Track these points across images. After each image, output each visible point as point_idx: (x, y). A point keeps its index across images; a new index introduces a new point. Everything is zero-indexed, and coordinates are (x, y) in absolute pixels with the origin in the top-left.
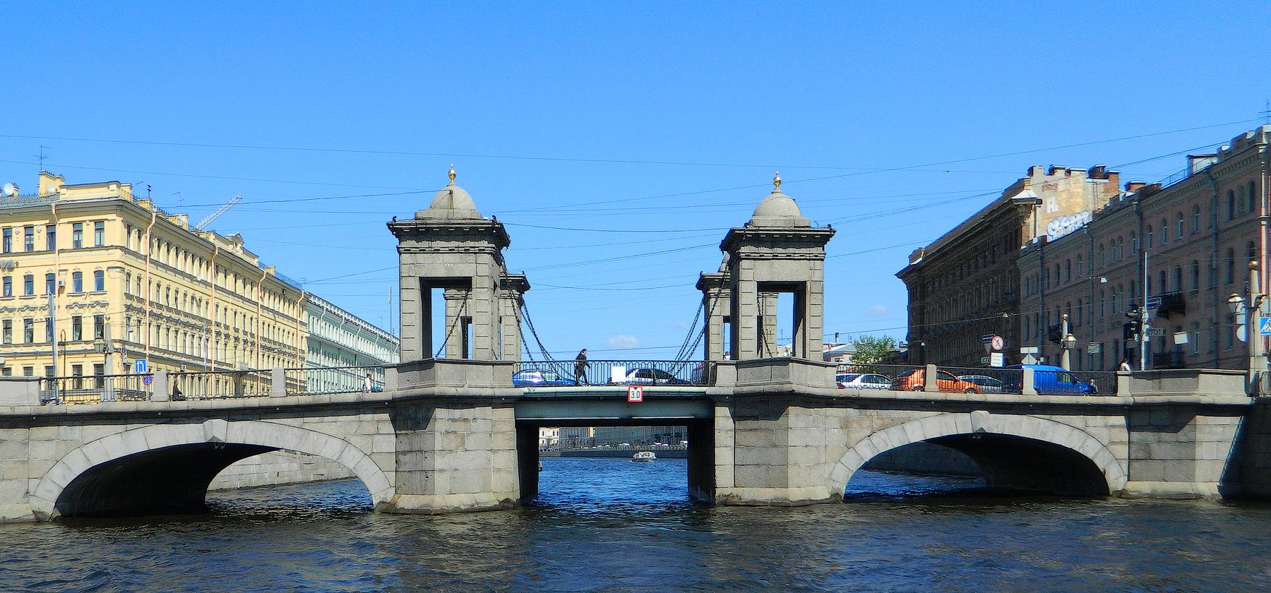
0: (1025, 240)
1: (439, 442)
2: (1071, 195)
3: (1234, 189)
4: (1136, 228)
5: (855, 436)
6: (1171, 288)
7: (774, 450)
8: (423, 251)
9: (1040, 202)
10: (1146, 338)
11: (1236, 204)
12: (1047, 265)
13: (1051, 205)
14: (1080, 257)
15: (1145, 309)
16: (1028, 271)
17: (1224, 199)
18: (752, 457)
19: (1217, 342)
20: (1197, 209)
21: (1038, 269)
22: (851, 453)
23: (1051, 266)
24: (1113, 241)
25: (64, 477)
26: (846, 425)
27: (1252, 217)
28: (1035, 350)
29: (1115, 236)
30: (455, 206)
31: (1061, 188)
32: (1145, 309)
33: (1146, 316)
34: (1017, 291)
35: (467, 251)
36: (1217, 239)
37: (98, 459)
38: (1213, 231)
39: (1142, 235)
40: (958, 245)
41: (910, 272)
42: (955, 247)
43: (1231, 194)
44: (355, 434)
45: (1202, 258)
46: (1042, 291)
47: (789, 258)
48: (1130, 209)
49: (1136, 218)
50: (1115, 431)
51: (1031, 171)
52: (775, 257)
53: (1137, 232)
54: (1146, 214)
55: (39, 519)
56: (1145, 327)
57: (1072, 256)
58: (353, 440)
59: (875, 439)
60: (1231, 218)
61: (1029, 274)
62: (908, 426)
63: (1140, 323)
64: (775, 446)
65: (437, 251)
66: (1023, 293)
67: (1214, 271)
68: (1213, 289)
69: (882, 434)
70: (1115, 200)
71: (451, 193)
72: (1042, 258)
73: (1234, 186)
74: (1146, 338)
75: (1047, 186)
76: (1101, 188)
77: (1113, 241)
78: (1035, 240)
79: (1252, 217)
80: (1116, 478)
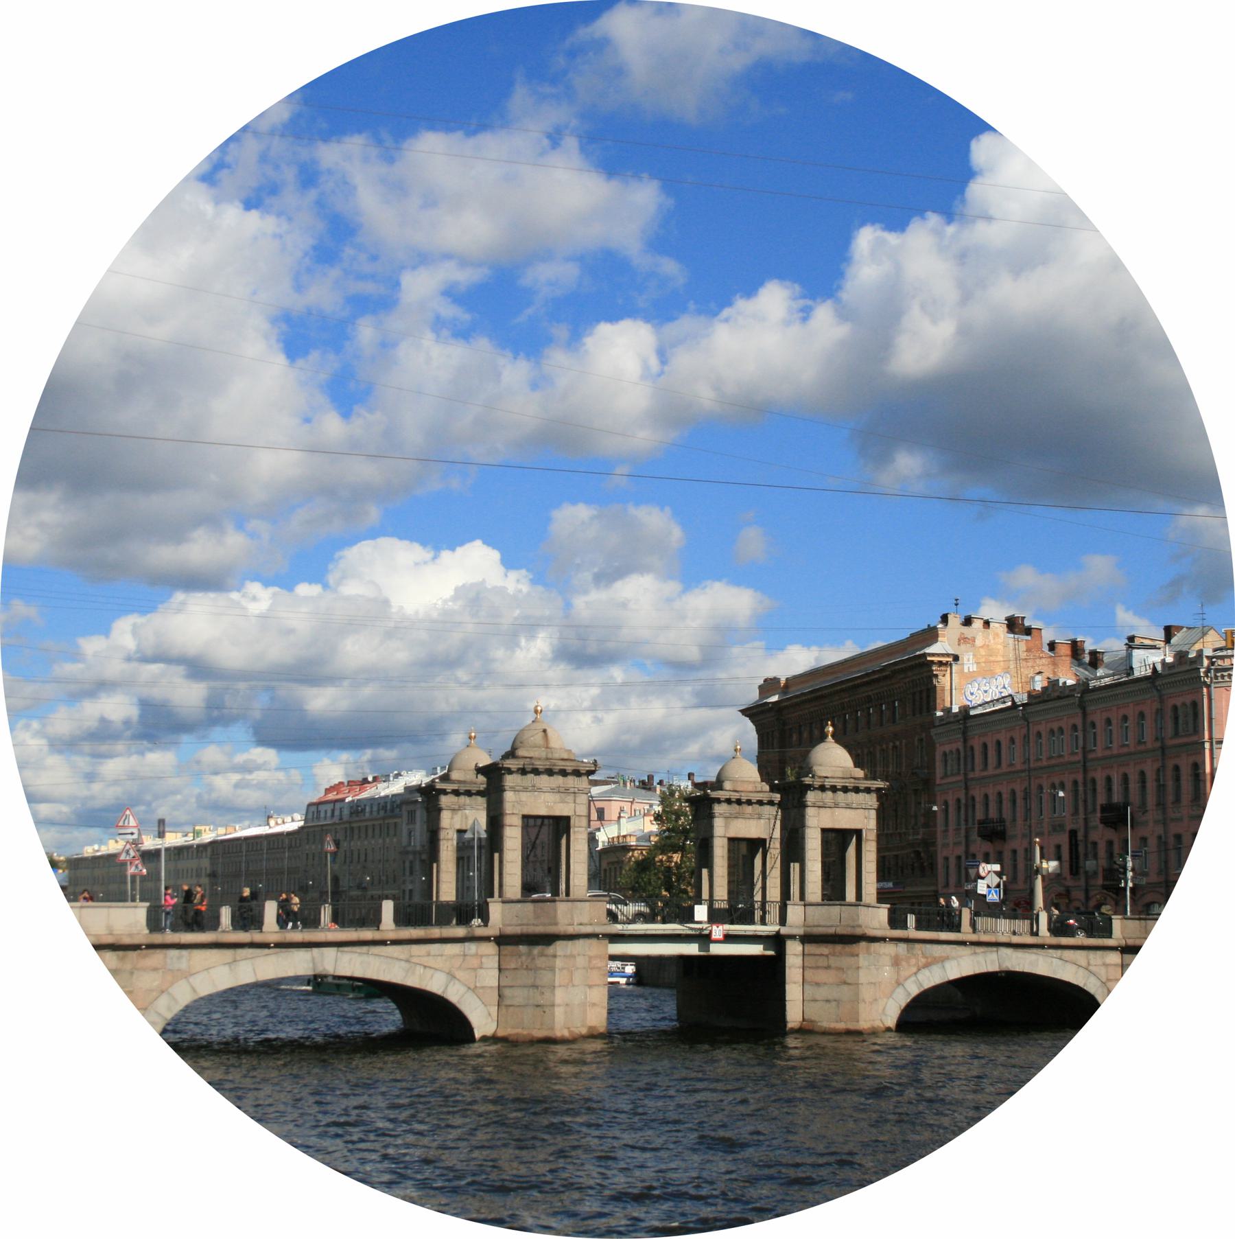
0: (939, 706)
1: (559, 978)
2: (991, 652)
3: (1179, 704)
4: (1078, 721)
5: (904, 973)
6: (1117, 798)
7: (845, 988)
8: (525, 789)
9: (956, 658)
10: (1130, 884)
11: (1180, 721)
12: (970, 743)
13: (969, 663)
14: (1012, 740)
15: (1129, 858)
16: (946, 745)
17: (1169, 714)
18: (822, 993)
19: (1166, 862)
20: (1142, 715)
21: (960, 745)
22: (900, 990)
23: (976, 744)
24: (1052, 732)
25: (169, 1009)
26: (896, 962)
27: (1194, 738)
28: (997, 867)
29: (1055, 726)
30: (552, 744)
31: (979, 642)
32: (1129, 858)
33: (1130, 864)
34: (931, 765)
35: (566, 791)
36: (1163, 754)
37: (205, 990)
38: (1158, 744)
39: (1084, 730)
40: (842, 690)
41: (762, 712)
42: (837, 692)
43: (1175, 708)
44: (460, 968)
45: (1150, 769)
46: (965, 774)
47: (848, 807)
48: (1071, 701)
49: (1079, 711)
50: (1111, 969)
51: (945, 619)
52: (836, 806)
53: (1080, 727)
54: (1090, 709)
55: (888, 1029)
56: (1130, 874)
57: (1003, 737)
58: (459, 974)
59: (920, 976)
60: (1176, 734)
61: (947, 748)
62: (947, 965)
63: (1125, 868)
64: (845, 983)
65: (540, 790)
66: (939, 771)
67: (1161, 788)
68: (1161, 804)
69: (926, 972)
70: (1053, 684)
71: (545, 731)
72: (964, 733)
73: (1178, 702)
74: (1130, 884)
75: (963, 640)
76: (1023, 646)
77: (1052, 732)
78: (955, 709)
79: (1194, 738)
80: (483, 1021)
